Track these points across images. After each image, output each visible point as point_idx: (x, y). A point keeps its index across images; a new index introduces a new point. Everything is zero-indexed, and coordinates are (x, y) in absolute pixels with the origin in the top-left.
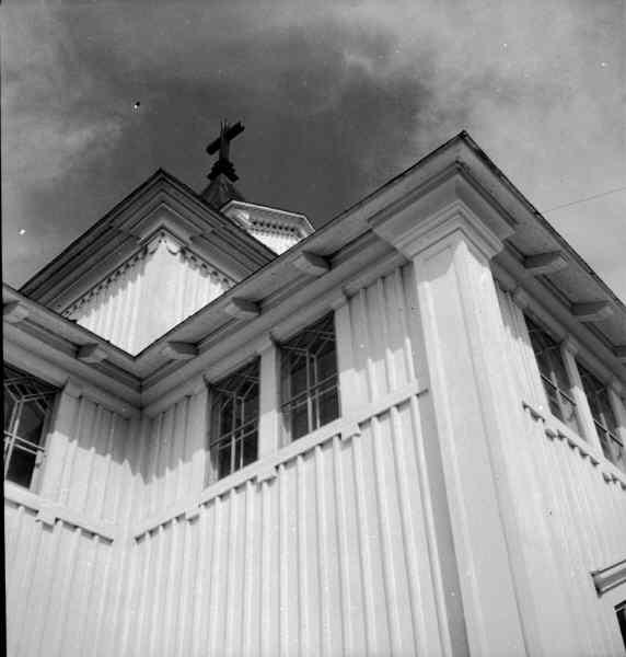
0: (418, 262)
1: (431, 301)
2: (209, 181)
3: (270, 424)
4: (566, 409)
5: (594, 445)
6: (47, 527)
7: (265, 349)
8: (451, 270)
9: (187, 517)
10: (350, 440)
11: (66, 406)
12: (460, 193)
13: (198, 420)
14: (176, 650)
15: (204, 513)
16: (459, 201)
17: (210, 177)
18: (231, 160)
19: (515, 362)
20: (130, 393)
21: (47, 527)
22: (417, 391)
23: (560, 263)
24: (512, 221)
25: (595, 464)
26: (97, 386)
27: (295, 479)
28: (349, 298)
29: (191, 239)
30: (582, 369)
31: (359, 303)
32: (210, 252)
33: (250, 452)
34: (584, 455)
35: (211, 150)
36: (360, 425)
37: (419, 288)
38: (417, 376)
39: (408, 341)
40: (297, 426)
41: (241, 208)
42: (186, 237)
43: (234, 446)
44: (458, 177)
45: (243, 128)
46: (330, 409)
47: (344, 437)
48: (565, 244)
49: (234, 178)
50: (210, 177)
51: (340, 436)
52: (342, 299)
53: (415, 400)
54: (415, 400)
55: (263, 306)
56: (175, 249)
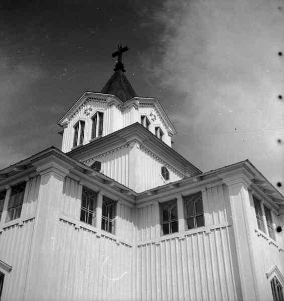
0: (230, 188)
1: (233, 201)
2: (114, 72)
3: (182, 223)
4: (262, 227)
5: (267, 236)
6: (98, 237)
7: (179, 197)
8: (239, 193)
9: (156, 243)
10: (208, 234)
11: (119, 208)
12: (244, 172)
13: (156, 213)
14: (196, 298)
15: (161, 243)
16: (243, 174)
17: (115, 70)
18: (123, 63)
19: (251, 211)
20: (133, 201)
21: (98, 237)
22: (228, 225)
23: (265, 184)
24: (254, 174)
25: (267, 240)
26: (128, 201)
27: (186, 240)
28: (207, 189)
29: (143, 142)
30: (265, 207)
31: (209, 191)
32: (147, 145)
33: (175, 229)
34: (265, 238)
35: (114, 55)
36: (211, 230)
37: (230, 197)
38: (228, 221)
39: (225, 210)
40: (190, 226)
41: (137, 99)
42: (141, 142)
43: (169, 226)
44: (243, 168)
45: (128, 49)
46: (201, 223)
47: (206, 233)
48: (267, 180)
49: (124, 71)
50: (115, 70)
51: (205, 232)
52: (205, 190)
53: (227, 227)
54: (227, 227)
55: (179, 185)
56: (138, 146)
